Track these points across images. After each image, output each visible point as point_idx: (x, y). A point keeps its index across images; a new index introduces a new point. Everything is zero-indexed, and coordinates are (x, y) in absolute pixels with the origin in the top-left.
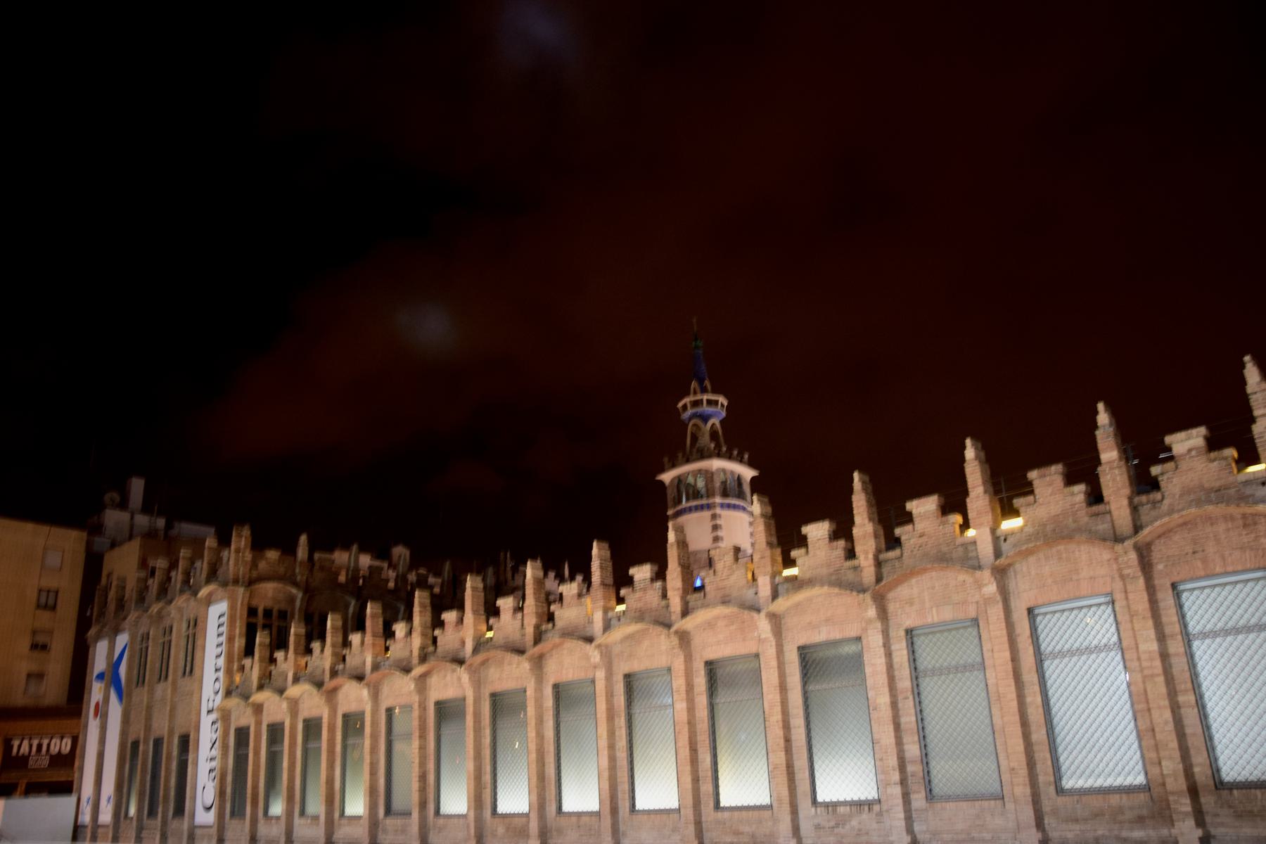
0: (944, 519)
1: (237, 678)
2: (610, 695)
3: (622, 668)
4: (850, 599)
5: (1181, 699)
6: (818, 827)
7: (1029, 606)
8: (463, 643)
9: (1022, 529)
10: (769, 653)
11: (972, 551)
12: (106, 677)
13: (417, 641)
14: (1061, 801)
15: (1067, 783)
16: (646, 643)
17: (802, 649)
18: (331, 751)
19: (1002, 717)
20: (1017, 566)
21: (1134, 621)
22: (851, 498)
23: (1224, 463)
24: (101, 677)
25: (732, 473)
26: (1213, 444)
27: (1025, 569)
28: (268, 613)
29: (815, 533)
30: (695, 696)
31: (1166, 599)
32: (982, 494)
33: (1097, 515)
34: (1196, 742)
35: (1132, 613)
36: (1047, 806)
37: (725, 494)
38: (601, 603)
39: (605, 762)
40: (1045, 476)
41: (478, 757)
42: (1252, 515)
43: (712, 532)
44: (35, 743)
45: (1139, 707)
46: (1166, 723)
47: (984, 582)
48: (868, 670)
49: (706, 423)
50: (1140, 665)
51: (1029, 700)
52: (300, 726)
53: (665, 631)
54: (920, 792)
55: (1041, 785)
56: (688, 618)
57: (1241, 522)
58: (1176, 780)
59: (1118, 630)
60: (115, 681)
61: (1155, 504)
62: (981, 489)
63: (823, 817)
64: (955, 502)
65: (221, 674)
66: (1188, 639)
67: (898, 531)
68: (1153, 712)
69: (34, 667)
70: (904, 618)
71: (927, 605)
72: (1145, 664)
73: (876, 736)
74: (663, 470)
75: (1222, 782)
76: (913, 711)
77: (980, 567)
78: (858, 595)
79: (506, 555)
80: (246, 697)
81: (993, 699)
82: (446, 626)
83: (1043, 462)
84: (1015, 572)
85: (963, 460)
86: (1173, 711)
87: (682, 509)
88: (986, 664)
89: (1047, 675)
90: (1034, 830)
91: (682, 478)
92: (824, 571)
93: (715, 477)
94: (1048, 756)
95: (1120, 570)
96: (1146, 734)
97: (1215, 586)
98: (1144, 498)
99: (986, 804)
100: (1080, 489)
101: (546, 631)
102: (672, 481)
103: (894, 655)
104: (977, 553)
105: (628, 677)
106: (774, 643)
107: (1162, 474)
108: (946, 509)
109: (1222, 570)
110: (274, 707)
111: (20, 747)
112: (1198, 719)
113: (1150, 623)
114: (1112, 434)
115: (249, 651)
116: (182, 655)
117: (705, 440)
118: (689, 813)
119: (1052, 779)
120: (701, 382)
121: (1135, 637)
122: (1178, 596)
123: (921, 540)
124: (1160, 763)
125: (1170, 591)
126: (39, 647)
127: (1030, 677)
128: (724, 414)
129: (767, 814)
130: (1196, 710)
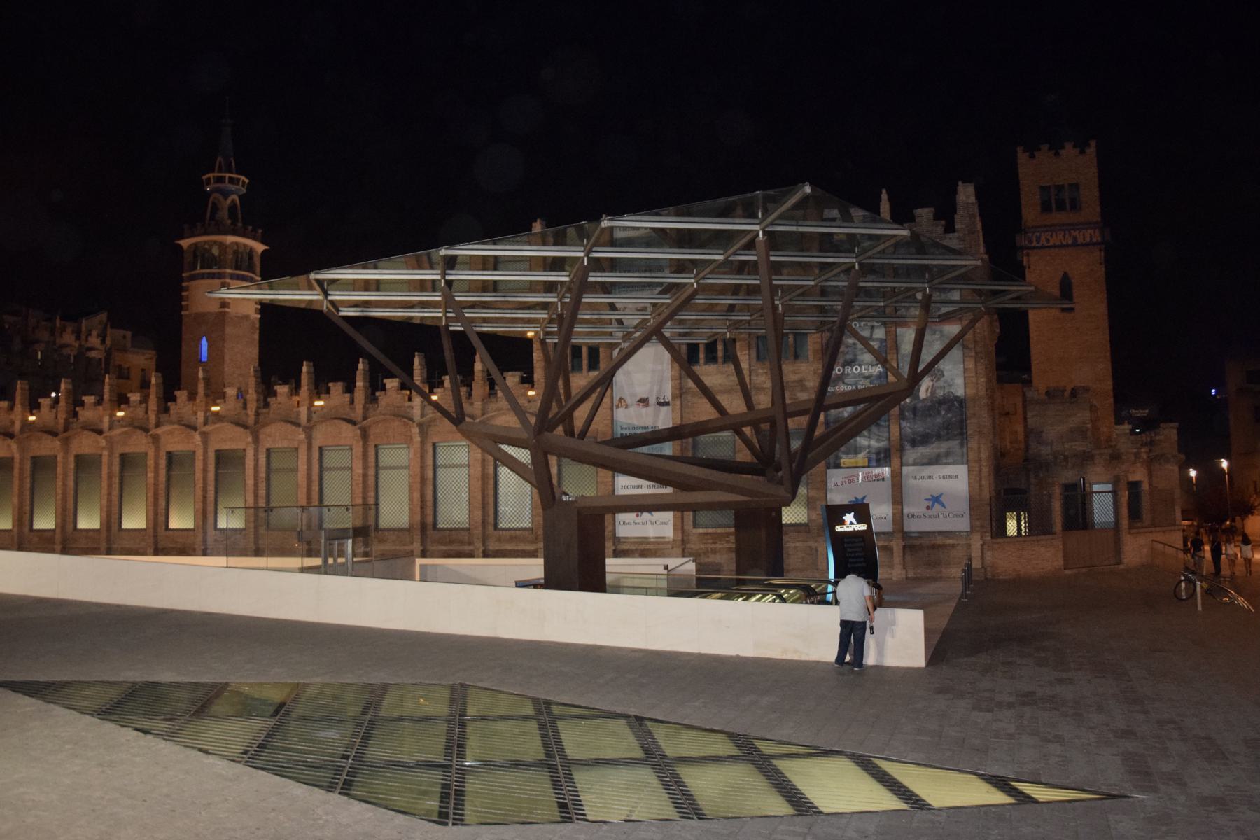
2: (110, 465)
3: (120, 449)
4: (241, 430)
6: (216, 540)
7: (320, 445)
8: (13, 423)
10: (200, 453)
17: (217, 451)
20: (318, 426)
25: (245, 246)
38: (109, 412)
39: (105, 502)
41: (21, 495)
48: (247, 466)
49: (226, 199)
53: (144, 434)
56: (158, 429)
62: (306, 388)
67: (269, 399)
70: (267, 443)
74: (182, 238)
93: (228, 250)
98: (371, 405)
102: (190, 246)
106: (202, 447)
117: (224, 214)
118: (151, 532)
125: (373, 448)
129: (192, 533)
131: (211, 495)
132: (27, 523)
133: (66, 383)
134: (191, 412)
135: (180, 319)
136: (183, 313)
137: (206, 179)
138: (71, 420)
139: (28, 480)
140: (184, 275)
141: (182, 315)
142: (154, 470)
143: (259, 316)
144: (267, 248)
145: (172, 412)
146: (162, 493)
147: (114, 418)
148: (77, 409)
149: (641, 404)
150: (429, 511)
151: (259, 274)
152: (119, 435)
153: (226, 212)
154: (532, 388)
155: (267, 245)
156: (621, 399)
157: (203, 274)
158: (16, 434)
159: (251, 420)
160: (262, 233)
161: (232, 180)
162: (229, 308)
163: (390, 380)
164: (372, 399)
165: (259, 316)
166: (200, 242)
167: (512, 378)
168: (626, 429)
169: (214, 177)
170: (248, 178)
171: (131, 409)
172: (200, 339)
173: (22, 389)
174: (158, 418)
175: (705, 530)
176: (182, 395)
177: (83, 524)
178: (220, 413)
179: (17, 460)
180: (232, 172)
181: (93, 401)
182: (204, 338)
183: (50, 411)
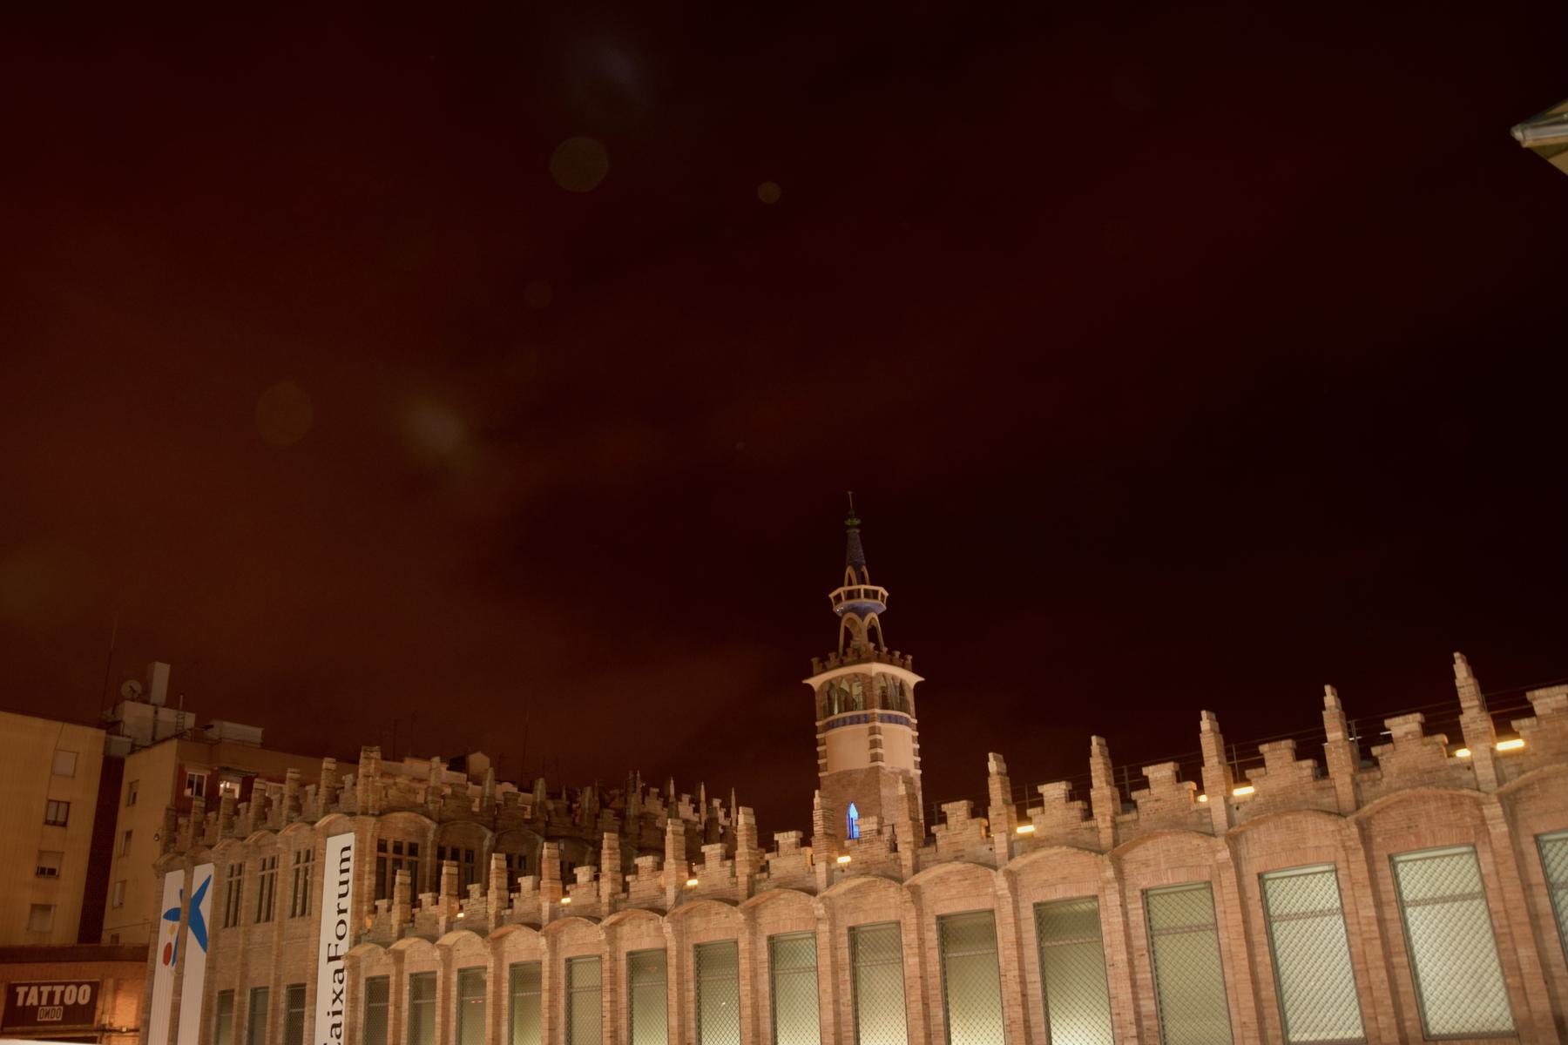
0: (1179, 785)
1: (369, 922)
4: (1087, 859)
5: (1396, 960)
7: (1259, 871)
8: (663, 891)
9: (1254, 796)
11: (1206, 817)
12: (182, 916)
13: (606, 887)
15: (1294, 1036)
19: (1234, 975)
20: (1249, 834)
21: (1356, 888)
23: (1435, 747)
24: (173, 915)
25: (894, 678)
26: (1428, 729)
27: (1255, 836)
28: (398, 848)
29: (1051, 793)
30: (927, 950)
31: (1384, 869)
32: (1217, 764)
33: (1323, 789)
34: (1407, 999)
35: (1354, 881)
37: (885, 706)
40: (1275, 750)
42: (1459, 795)
43: (871, 748)
44: (46, 990)
45: (1358, 967)
46: (1382, 982)
47: (1219, 848)
48: (1104, 928)
50: (1360, 929)
51: (1258, 959)
52: (455, 978)
55: (1269, 1039)
57: (1449, 802)
58: (1390, 1033)
59: (1340, 895)
60: (196, 922)
61: (1375, 782)
62: (1215, 760)
64: (1190, 770)
65: (346, 917)
66: (1402, 905)
67: (1134, 795)
68: (1371, 971)
69: (40, 899)
70: (1141, 879)
71: (1163, 867)
72: (1364, 928)
73: (1113, 992)
74: (811, 675)
75: (1429, 1035)
76: (1148, 969)
77: (1213, 835)
78: (1097, 856)
79: (635, 773)
80: (386, 945)
81: (1224, 958)
82: (640, 871)
83: (1274, 736)
84: (1246, 838)
85: (1199, 730)
86: (1388, 971)
87: (833, 721)
88: (1219, 924)
89: (1276, 936)
91: (833, 682)
92: (1061, 831)
93: (875, 683)
94: (1276, 1011)
95: (1343, 842)
96: (1364, 993)
97: (1426, 859)
98: (1365, 776)
100: (1308, 764)
101: (760, 881)
103: (1130, 913)
104: (1211, 819)
105: (852, 931)
106: (1010, 900)
107: (1382, 754)
108: (1181, 777)
109: (1433, 845)
110: (419, 955)
111: (26, 994)
112: (1410, 978)
113: (1369, 891)
114: (1338, 715)
115: (383, 889)
116: (290, 893)
117: (861, 639)
120: (857, 568)
121: (1356, 905)
122: (1394, 866)
123: (1157, 805)
124: (1376, 1018)
125: (1387, 862)
126: (46, 872)
128: (884, 608)
130: (1408, 970)
131: (1035, 990)
134: (978, 838)
136: (820, 775)
138: (758, 876)
139: (692, 986)
140: (818, 724)
141: (819, 778)
143: (920, 772)
144: (922, 679)
145: (940, 842)
146: (935, 994)
147: (833, 866)
151: (914, 715)
157: (844, 719)
158: (668, 908)
159: (1106, 836)
161: (867, 594)
164: (1365, 758)
166: (835, 678)
169: (844, 592)
170: (888, 592)
171: (863, 847)
173: (674, 833)
174: (916, 857)
176: (957, 810)
179: (672, 953)
181: (793, 840)
183: (723, 866)
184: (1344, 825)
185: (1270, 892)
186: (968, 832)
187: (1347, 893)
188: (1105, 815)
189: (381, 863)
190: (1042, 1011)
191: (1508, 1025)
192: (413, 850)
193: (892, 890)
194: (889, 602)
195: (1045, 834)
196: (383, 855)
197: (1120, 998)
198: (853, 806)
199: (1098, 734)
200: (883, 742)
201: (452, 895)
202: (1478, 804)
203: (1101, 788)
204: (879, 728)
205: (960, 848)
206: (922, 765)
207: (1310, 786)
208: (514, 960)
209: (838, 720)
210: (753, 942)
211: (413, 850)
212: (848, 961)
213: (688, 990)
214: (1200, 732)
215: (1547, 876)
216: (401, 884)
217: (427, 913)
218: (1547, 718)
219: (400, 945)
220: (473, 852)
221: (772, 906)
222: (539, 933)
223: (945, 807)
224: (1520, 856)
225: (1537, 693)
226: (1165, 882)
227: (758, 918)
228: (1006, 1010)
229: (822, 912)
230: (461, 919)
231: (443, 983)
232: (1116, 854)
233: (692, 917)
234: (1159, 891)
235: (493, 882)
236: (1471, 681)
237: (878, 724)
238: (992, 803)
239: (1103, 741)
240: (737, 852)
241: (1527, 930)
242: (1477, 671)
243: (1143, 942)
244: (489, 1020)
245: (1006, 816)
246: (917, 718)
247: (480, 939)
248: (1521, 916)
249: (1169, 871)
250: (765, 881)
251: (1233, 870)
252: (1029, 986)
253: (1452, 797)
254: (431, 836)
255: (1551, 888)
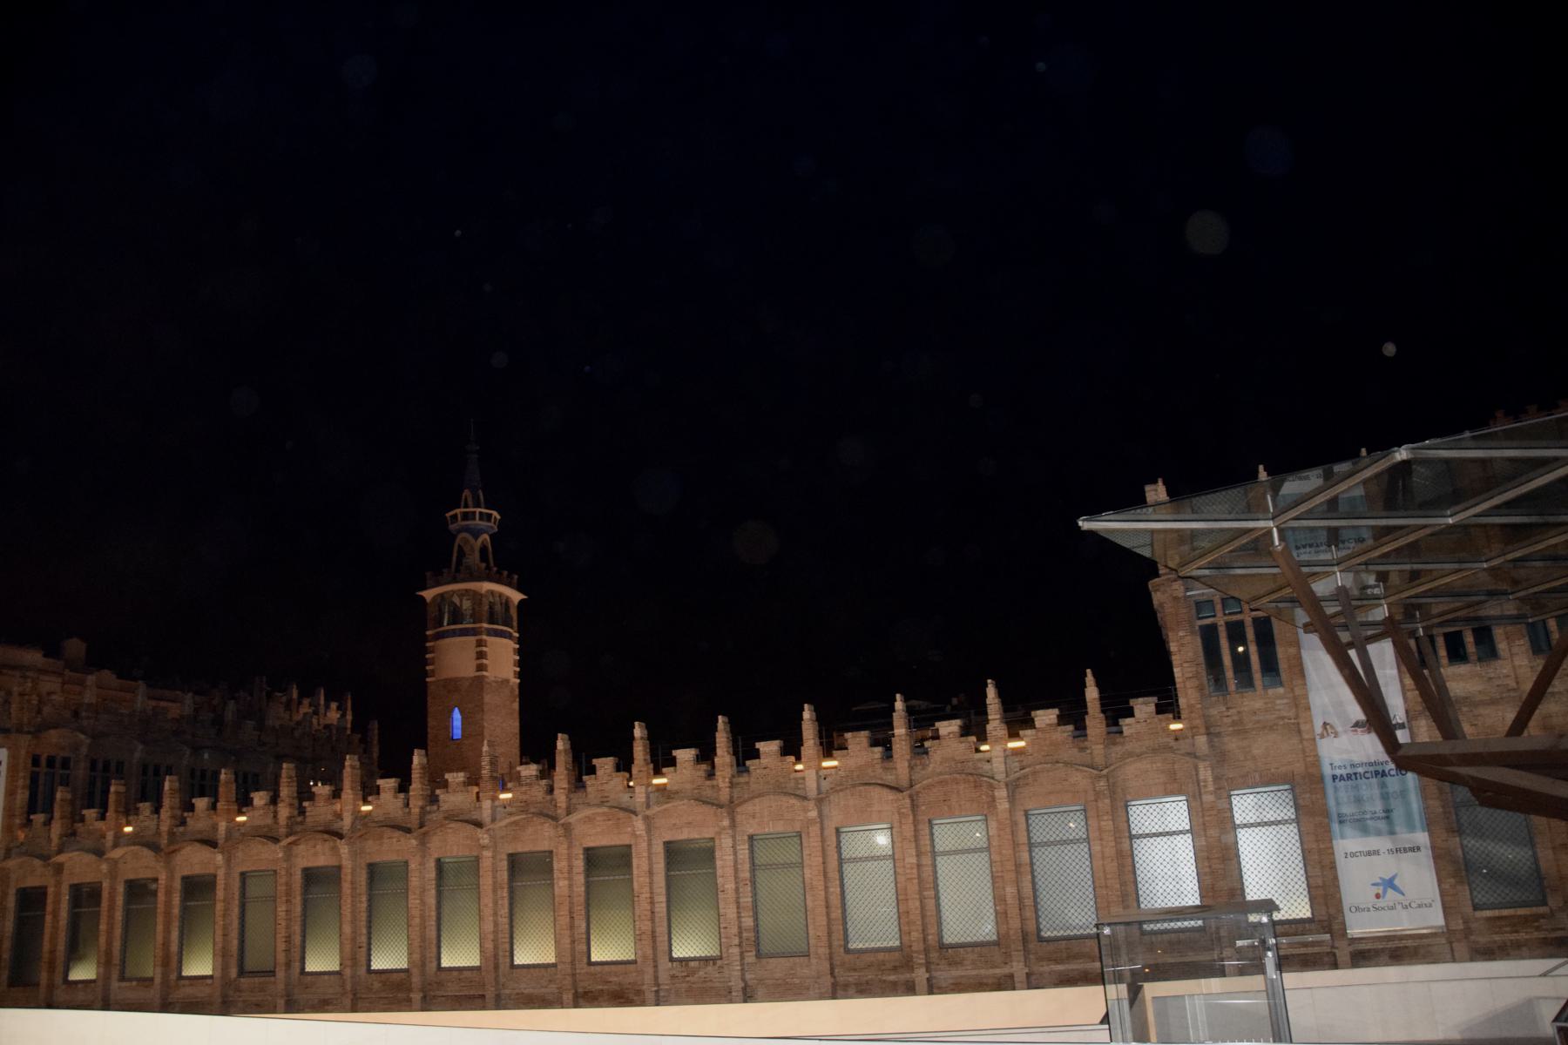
6: (673, 977)
7: (837, 826)
8: (339, 816)
11: (801, 784)
13: (284, 812)
14: (848, 958)
16: (530, 830)
18: (168, 914)
20: (832, 797)
22: (715, 734)
25: (501, 595)
28: (51, 762)
29: (683, 756)
34: (932, 920)
36: (837, 961)
46: (916, 908)
48: (719, 863)
52: (121, 889)
54: (751, 951)
56: (571, 816)
57: (972, 785)
61: (924, 767)
62: (811, 742)
63: (677, 970)
64: (792, 748)
66: (934, 854)
73: (722, 911)
74: (425, 588)
75: (943, 944)
76: (750, 894)
77: (805, 798)
80: (45, 858)
82: (317, 798)
85: (801, 719)
90: (829, 976)
91: (445, 595)
93: (484, 599)
96: (902, 915)
99: (797, 960)
102: (434, 598)
106: (646, 838)
110: (79, 866)
113: (913, 845)
117: (474, 559)
119: (842, 943)
125: (927, 825)
127: (833, 875)
132: (363, 960)
133: (419, 755)
135: (424, 687)
137: (451, 517)
138: (428, 808)
139: (364, 899)
142: (569, 877)
143: (518, 681)
144: (525, 597)
145: (589, 789)
148: (438, 792)
149: (1359, 730)
150: (1029, 913)
152: (506, 826)
153: (477, 554)
154: (1177, 718)
155: (524, 593)
156: (1325, 724)
160: (518, 579)
162: (486, 671)
163: (945, 723)
164: (919, 749)
165: (518, 681)
166: (446, 592)
167: (1144, 707)
168: (1340, 767)
170: (500, 515)
171: (524, 788)
172: (452, 711)
173: (352, 767)
175: (1496, 913)
177: (451, 959)
178: (669, 787)
180: (480, 507)
182: (456, 710)
184: (901, 798)
185: (843, 841)
186: (612, 783)
187: (898, 845)
188: (725, 778)
189: (34, 779)
190: (665, 924)
191: (995, 937)
192: (65, 763)
193: (547, 825)
194: (501, 524)
195: (675, 788)
196: (36, 769)
197: (727, 916)
198: (456, 710)
199: (723, 715)
200: (488, 654)
201: (119, 812)
202: (992, 788)
203: (723, 756)
204: (486, 641)
205: (606, 795)
206: (520, 675)
207: (878, 766)
208: (186, 873)
209: (448, 631)
210: (422, 864)
211: (65, 763)
212: (506, 880)
213: (361, 902)
214: (802, 720)
215: (1029, 838)
216: (62, 800)
217: (91, 828)
218: (1042, 730)
219: (61, 858)
220: (122, 763)
221: (440, 834)
222: (216, 850)
223: (595, 761)
224: (1014, 824)
225: (1039, 712)
226: (767, 830)
227: (428, 843)
228: (637, 923)
229: (486, 841)
230: (129, 834)
231: (110, 893)
232: (731, 807)
233: (366, 840)
234: (761, 837)
235: (166, 802)
236: (997, 701)
237: (484, 637)
238: (636, 762)
239: (726, 720)
240: (411, 787)
241: (1013, 875)
242: (1001, 694)
243: (747, 875)
244: (160, 928)
245: (645, 773)
246: (518, 632)
247: (153, 854)
248: (1010, 866)
249: (771, 823)
250: (434, 812)
251: (818, 825)
252: (657, 905)
253: (975, 782)
254: (84, 750)
255: (1031, 846)
